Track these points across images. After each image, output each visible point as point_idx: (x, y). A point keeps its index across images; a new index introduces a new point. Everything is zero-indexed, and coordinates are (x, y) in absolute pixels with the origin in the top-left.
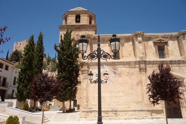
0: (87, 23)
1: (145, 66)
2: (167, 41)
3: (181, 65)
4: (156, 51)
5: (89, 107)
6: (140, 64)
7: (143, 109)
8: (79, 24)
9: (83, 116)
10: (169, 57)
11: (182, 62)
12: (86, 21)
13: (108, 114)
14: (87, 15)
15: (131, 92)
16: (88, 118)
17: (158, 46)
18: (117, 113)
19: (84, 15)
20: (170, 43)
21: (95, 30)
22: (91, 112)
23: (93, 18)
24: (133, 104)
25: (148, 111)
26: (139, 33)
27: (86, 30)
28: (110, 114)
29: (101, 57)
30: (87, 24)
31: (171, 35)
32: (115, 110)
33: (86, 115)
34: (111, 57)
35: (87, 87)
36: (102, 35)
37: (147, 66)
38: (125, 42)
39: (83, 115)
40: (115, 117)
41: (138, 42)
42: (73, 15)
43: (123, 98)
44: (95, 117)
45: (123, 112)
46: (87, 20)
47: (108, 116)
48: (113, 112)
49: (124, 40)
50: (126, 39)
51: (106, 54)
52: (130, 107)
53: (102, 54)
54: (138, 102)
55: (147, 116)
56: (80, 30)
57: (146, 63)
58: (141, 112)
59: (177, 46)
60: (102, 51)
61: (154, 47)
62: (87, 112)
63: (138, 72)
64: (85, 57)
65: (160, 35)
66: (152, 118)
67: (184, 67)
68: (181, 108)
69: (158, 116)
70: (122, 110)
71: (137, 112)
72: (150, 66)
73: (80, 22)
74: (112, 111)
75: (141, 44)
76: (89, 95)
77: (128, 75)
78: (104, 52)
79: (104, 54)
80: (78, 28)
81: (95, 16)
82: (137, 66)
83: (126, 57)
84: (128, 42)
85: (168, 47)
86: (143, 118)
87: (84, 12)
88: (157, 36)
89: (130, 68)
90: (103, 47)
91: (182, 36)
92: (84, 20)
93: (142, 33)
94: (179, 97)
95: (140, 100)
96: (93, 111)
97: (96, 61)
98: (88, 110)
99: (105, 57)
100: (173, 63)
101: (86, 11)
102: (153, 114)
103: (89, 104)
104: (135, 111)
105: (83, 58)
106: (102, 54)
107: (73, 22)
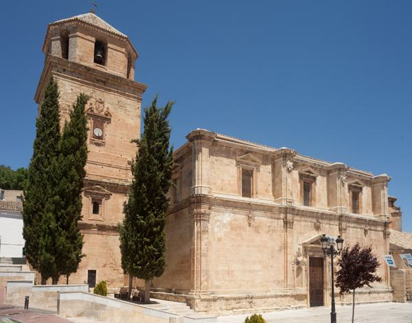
3: (332, 222)
4: (301, 192)
5: (210, 290)
6: (286, 213)
8: (98, 68)
12: (121, 68)
14: (123, 50)
15: (271, 264)
18: (254, 300)
19: (119, 48)
20: (319, 179)
22: (215, 300)
27: (121, 94)
28: (244, 303)
32: (251, 295)
35: (207, 251)
36: (224, 137)
41: (285, 169)
43: (260, 273)
44: (221, 309)
54: (279, 282)
56: (106, 89)
58: (283, 299)
59: (326, 188)
61: (300, 182)
62: (208, 300)
63: (282, 228)
68: (325, 291)
74: (246, 298)
77: (269, 231)
80: (101, 81)
86: (277, 309)
87: (120, 42)
89: (272, 218)
91: (282, 159)
95: (282, 277)
100: (324, 217)
101: (123, 37)
104: (276, 296)
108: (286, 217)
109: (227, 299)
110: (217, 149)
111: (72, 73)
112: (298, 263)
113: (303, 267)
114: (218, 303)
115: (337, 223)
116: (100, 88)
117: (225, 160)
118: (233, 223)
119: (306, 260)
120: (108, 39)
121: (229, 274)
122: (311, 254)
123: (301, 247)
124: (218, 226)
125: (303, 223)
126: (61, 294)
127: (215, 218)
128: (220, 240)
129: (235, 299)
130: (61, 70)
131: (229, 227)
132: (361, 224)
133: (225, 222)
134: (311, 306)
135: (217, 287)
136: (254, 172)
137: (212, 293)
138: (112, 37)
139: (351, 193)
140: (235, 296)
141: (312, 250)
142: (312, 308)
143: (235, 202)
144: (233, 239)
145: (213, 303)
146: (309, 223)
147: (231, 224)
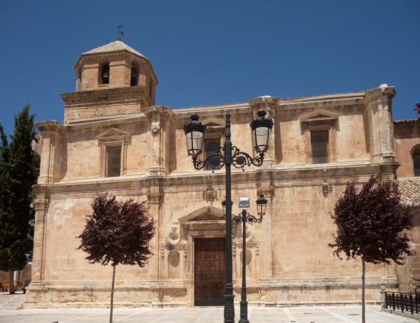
0: (125, 83)
1: (271, 184)
2: (334, 118)
7: (273, 285)
8: (106, 88)
9: (31, 300)
10: (335, 160)
11: (244, 178)
12: (122, 79)
13: (76, 295)
14: (124, 62)
16: (39, 305)
17: (311, 132)
18: (94, 293)
19: (90, 66)
21: (140, 101)
22: (45, 291)
23: (140, 70)
24: (129, 275)
25: (154, 290)
26: (154, 109)
27: (120, 103)
28: (81, 295)
29: (232, 161)
30: (123, 86)
31: (237, 110)
33: (35, 298)
34: (252, 163)
37: (165, 191)
38: (133, 134)
39: (30, 299)
40: (90, 303)
42: (94, 65)
44: (52, 301)
45: (105, 293)
46: (124, 75)
47: (75, 301)
48: (86, 292)
49: (133, 128)
50: (137, 126)
51: (241, 155)
52: (122, 282)
53: (234, 156)
55: (150, 301)
57: (165, 183)
58: (140, 293)
60: (234, 148)
62: (38, 291)
64: (199, 163)
65: (212, 112)
66: (162, 306)
67: (247, 191)
69: (177, 301)
70: (102, 287)
71: (132, 293)
72: (172, 189)
73: (108, 83)
74: (84, 290)
75: (157, 138)
76: (47, 257)
78: (238, 150)
79: (237, 156)
80: (103, 98)
81: (148, 61)
82: (144, 190)
83: (132, 169)
84: (140, 133)
85: (338, 132)
88: (205, 115)
90: (88, 147)
92: (119, 77)
93: (161, 110)
94: (108, 259)
96: (49, 289)
97: (223, 171)
98: (40, 288)
99: (241, 161)
102: (167, 297)
103: (46, 276)
105: (195, 165)
106: (234, 156)
107: (93, 83)
108: (149, 191)
109: (60, 291)
110: (76, 134)
111: (79, 101)
112: (170, 247)
113: (182, 253)
114: (49, 295)
115: (254, 185)
116: (102, 104)
117: (86, 143)
118: (76, 208)
119: (189, 243)
120: (110, 59)
121: (68, 263)
122: (196, 234)
123: (178, 226)
124: (58, 214)
125: (182, 195)
126: (221, 309)
127: (56, 206)
128: (59, 228)
129: (70, 291)
130: (71, 102)
131: (71, 214)
132: (311, 178)
133: (66, 209)
134: (195, 305)
135: (54, 277)
136: (122, 147)
137: (48, 284)
138: (111, 56)
139: (308, 134)
140: (69, 287)
141: (197, 228)
142: (198, 308)
143: (78, 186)
144: (75, 225)
145: (43, 294)
146: (194, 193)
147: (73, 209)
